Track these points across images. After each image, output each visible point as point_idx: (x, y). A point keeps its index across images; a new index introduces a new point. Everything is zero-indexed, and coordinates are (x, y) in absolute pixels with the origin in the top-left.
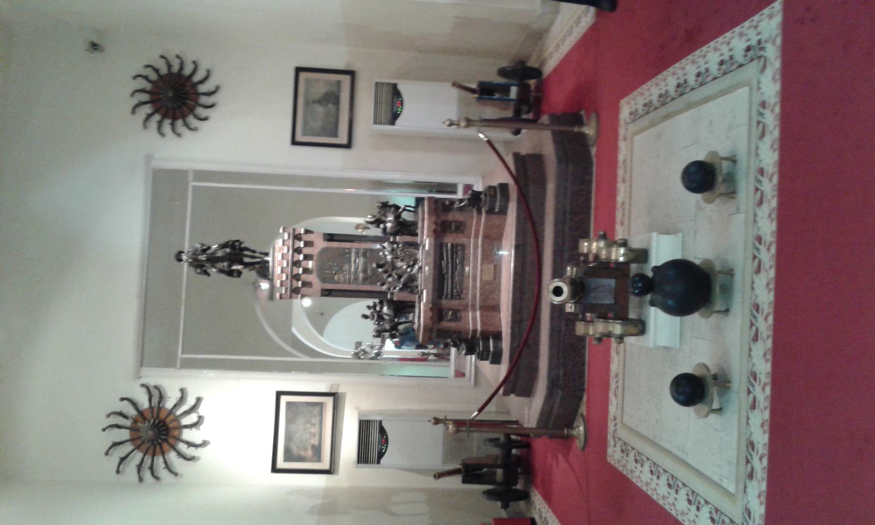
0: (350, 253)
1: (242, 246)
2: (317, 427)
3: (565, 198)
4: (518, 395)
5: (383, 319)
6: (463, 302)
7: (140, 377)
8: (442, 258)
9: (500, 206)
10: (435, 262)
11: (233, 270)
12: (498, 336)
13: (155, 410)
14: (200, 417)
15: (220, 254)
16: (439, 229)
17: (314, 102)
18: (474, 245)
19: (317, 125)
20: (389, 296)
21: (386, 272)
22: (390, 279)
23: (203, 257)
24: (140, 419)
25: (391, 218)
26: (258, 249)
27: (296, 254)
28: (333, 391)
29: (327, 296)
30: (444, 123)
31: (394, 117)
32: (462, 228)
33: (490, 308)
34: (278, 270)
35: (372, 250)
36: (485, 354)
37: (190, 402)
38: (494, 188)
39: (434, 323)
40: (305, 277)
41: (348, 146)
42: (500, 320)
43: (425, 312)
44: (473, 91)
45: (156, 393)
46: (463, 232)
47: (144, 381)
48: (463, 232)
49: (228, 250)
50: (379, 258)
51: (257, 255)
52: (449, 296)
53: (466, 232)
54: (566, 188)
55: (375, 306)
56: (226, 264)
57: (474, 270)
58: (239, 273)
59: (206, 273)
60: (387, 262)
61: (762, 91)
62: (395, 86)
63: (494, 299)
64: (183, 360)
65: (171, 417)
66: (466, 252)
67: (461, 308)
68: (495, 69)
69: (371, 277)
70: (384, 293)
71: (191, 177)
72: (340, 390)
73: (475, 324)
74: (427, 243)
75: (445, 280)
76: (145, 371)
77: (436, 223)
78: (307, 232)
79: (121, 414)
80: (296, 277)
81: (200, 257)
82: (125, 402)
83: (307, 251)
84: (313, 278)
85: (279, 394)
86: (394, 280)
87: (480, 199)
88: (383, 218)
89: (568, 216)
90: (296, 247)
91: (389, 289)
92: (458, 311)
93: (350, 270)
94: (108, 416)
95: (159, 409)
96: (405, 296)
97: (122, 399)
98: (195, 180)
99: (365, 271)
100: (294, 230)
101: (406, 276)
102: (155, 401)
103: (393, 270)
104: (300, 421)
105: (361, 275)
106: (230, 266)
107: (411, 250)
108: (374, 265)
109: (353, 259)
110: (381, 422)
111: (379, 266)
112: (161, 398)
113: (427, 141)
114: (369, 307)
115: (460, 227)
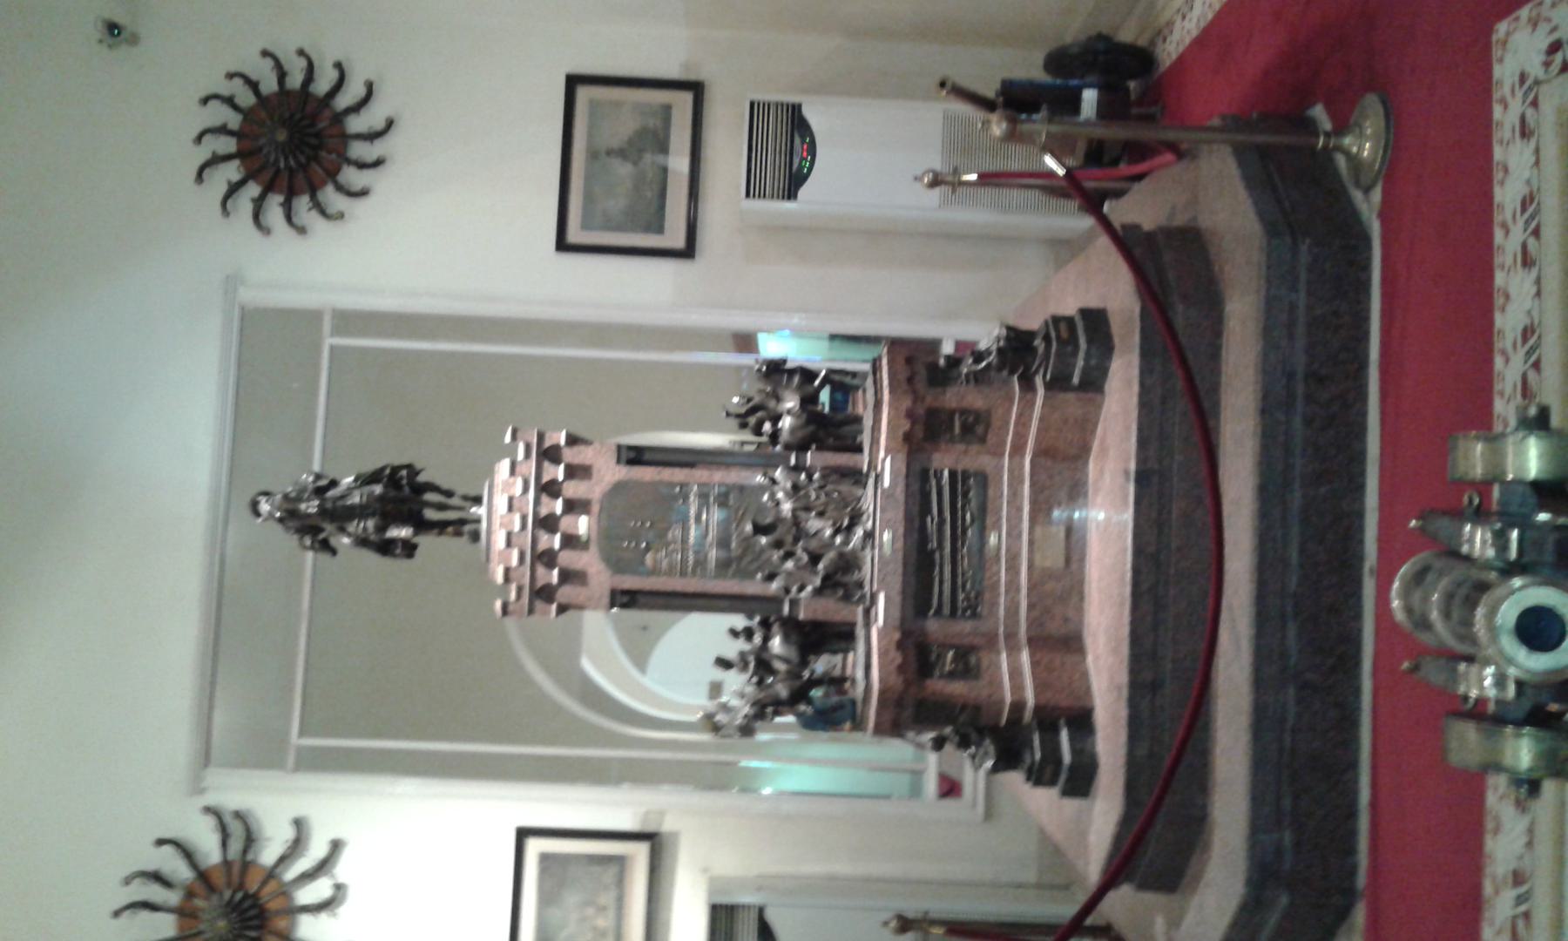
0: (686, 498)
1: (421, 478)
2: (611, 913)
3: (1291, 337)
4: (1143, 886)
5: (773, 672)
6: (984, 626)
7: (201, 791)
8: (925, 509)
9: (1086, 372)
10: (908, 519)
11: (393, 541)
12: (1082, 722)
13: (236, 869)
14: (339, 887)
15: (356, 499)
16: (919, 432)
17: (609, 153)
18: (1012, 476)
19: (616, 204)
20: (786, 609)
21: (778, 544)
22: (790, 565)
23: (311, 507)
24: (200, 888)
25: (791, 402)
26: (461, 490)
27: (545, 498)
28: (650, 828)
29: (624, 606)
30: (918, 179)
31: (793, 184)
32: (980, 429)
33: (1059, 642)
34: (499, 541)
35: (742, 489)
36: (1049, 771)
37: (317, 850)
38: (1070, 321)
39: (908, 684)
40: (568, 558)
41: (688, 252)
42: (1085, 675)
43: (882, 655)
44: (987, 105)
45: (239, 829)
46: (982, 440)
47: (211, 799)
48: (982, 440)
49: (378, 489)
50: (762, 508)
51: (455, 501)
52: (946, 610)
53: (991, 439)
54: (1293, 307)
55: (748, 633)
56: (370, 524)
57: (1010, 540)
58: (409, 549)
59: (326, 547)
60: (779, 520)
61: (1525, 191)
62: (795, 111)
63: (1066, 620)
64: (300, 751)
65: (271, 887)
66: (991, 492)
67: (977, 641)
68: (1039, 57)
69: (740, 558)
70: (776, 601)
71: (327, 326)
72: (667, 826)
73: (1017, 687)
74: (885, 465)
75: (936, 569)
76: (214, 777)
77: (910, 415)
78: (573, 440)
79: (157, 877)
80: (547, 558)
81: (303, 506)
82: (167, 849)
83: (573, 489)
84: (589, 561)
85: (523, 834)
86: (798, 567)
87: (1034, 350)
88: (772, 404)
89: (1300, 389)
90: (546, 478)
91: (787, 591)
92: (972, 649)
93: (685, 540)
94: (128, 881)
95: (246, 865)
96: (830, 609)
97: (161, 842)
98: (336, 331)
99: (723, 543)
100: (541, 437)
101: (830, 556)
102: (235, 846)
103: (796, 540)
104: (572, 899)
105: (713, 554)
106: (381, 529)
107: (845, 487)
108: (749, 528)
109: (693, 512)
110: (761, 910)
111: (759, 530)
112: (250, 840)
113: (876, 239)
114: (734, 633)
115: (975, 428)
